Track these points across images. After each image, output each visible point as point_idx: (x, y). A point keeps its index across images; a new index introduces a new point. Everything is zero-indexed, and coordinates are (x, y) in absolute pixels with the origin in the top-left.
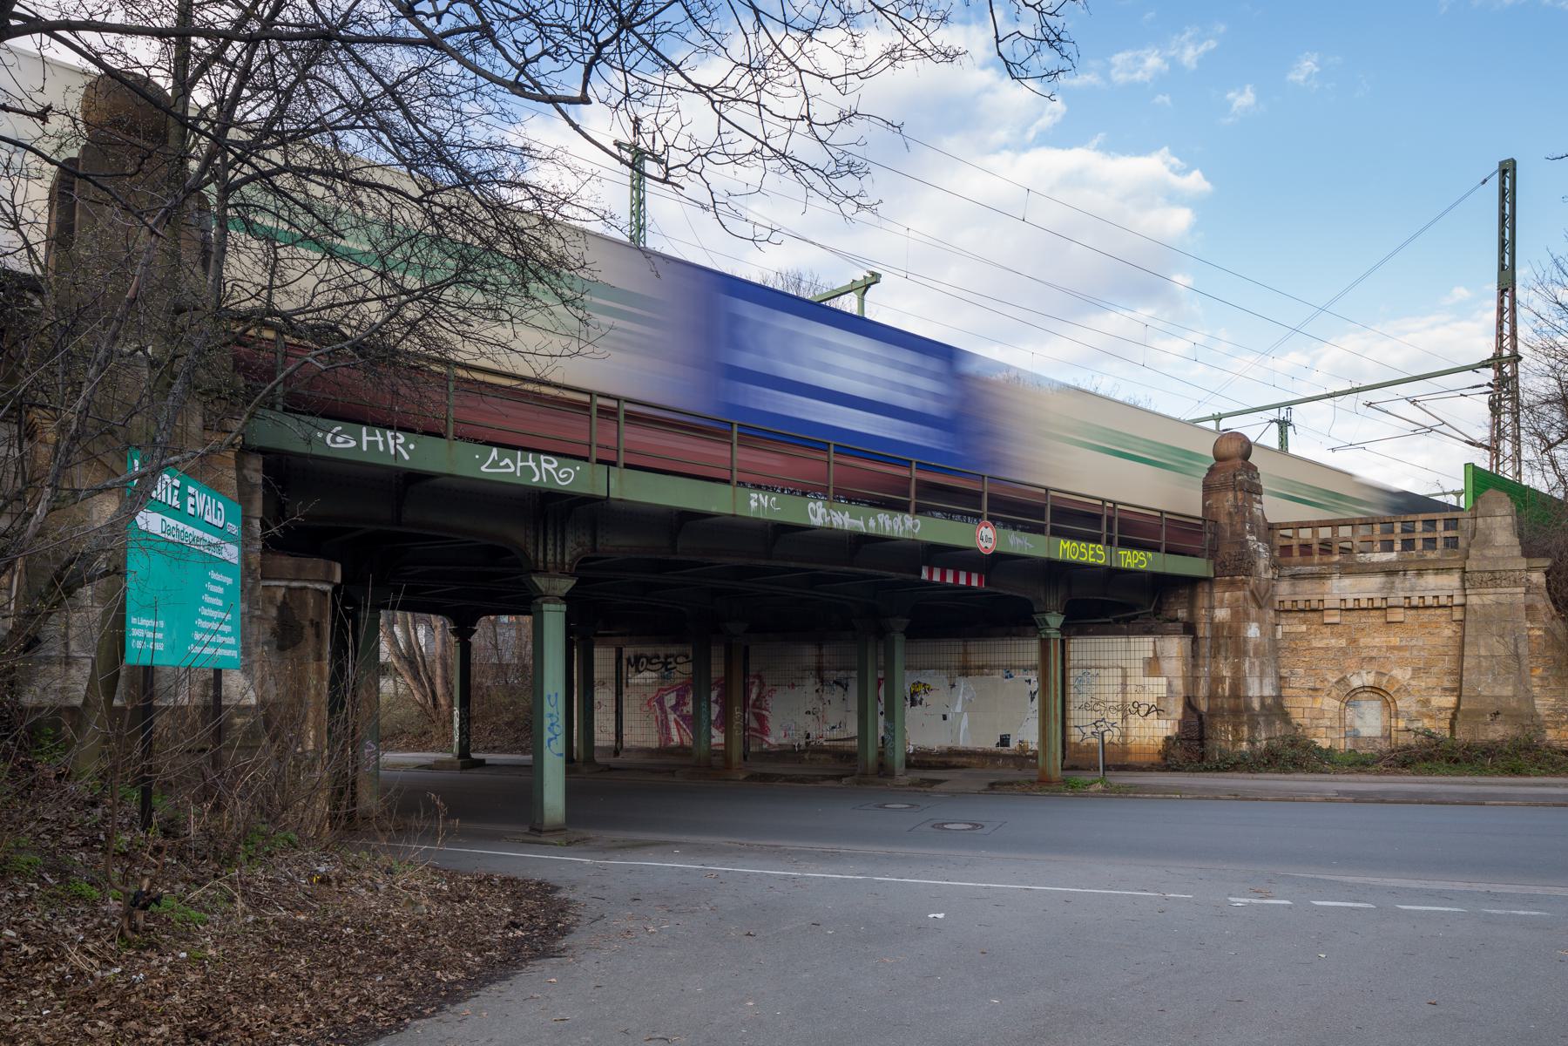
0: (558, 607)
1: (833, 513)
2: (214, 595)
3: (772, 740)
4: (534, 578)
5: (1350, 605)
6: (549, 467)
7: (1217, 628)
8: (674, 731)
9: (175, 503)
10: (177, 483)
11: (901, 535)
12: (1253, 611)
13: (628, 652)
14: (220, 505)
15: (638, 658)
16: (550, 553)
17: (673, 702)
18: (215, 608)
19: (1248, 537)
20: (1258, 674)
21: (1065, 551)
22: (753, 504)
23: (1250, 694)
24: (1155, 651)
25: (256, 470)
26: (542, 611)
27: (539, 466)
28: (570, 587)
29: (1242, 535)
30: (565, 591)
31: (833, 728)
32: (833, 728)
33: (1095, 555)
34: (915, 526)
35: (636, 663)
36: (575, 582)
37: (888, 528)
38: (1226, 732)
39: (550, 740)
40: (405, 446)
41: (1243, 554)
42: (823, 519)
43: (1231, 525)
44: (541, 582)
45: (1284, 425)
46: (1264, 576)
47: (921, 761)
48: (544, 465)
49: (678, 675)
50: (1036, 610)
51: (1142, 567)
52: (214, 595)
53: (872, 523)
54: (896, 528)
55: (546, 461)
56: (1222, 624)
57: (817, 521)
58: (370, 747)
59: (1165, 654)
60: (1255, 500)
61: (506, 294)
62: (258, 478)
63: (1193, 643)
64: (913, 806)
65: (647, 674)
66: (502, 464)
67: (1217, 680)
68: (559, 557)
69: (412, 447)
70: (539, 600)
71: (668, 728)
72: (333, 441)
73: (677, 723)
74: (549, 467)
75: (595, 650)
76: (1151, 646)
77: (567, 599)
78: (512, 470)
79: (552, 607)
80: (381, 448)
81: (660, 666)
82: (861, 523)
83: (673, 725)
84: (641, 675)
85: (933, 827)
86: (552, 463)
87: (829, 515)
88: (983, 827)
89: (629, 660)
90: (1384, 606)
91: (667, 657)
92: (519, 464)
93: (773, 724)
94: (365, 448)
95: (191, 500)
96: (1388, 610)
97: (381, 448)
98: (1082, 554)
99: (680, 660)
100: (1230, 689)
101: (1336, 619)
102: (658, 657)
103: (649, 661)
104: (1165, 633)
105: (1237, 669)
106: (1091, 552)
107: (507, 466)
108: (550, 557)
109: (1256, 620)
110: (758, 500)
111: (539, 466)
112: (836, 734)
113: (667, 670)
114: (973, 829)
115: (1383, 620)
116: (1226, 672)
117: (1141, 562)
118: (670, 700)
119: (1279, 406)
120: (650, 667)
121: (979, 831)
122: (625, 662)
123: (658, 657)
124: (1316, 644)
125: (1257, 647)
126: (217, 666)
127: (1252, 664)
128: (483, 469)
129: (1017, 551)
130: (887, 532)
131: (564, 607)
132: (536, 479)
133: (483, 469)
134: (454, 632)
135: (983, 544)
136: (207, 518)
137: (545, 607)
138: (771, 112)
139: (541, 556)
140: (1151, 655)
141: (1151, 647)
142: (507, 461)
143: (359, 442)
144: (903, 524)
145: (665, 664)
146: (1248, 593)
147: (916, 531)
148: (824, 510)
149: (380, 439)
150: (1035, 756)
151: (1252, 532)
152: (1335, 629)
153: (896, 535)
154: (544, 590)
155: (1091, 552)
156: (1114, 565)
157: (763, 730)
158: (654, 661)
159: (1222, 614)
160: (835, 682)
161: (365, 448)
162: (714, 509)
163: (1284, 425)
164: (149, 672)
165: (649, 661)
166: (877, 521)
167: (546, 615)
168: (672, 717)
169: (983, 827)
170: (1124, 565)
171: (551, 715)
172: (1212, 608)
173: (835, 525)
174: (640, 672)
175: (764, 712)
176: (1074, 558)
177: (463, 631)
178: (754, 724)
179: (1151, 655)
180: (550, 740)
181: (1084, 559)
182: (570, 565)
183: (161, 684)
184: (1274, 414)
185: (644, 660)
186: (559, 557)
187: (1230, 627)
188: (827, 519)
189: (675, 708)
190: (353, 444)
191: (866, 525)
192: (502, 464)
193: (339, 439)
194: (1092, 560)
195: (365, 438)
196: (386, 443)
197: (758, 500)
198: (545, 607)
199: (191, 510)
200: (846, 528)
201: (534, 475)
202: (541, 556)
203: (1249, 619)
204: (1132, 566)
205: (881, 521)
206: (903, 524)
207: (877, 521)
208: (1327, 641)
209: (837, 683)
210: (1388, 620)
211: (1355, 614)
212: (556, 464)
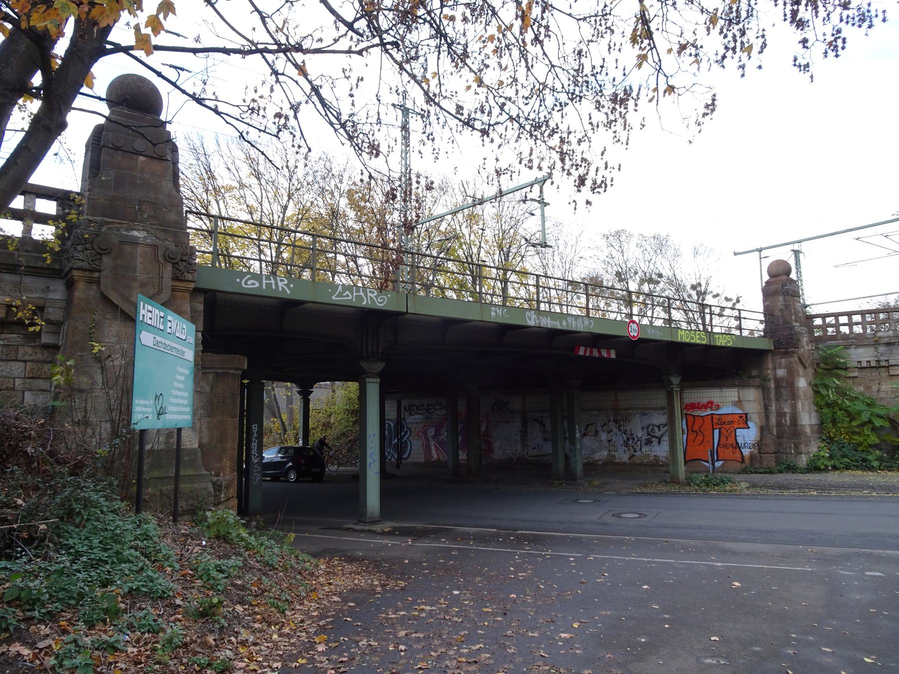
0: (375, 380)
1: (541, 318)
2: (179, 381)
3: (496, 457)
4: (361, 363)
5: (864, 365)
6: (372, 295)
7: (778, 381)
8: (434, 452)
9: (162, 327)
10: (162, 314)
11: (582, 330)
12: (801, 371)
13: (404, 403)
14: (184, 326)
15: (410, 406)
16: (370, 347)
17: (433, 433)
18: (179, 389)
19: (794, 324)
20: (807, 410)
21: (681, 337)
22: (493, 314)
23: (804, 423)
24: (739, 397)
25: (200, 303)
26: (365, 383)
27: (366, 295)
28: (142, 296)
29: (790, 323)
30: (379, 370)
31: (534, 448)
32: (534, 448)
33: (700, 339)
34: (590, 324)
35: (410, 409)
37: (574, 326)
38: (790, 448)
39: (371, 464)
40: (287, 285)
41: (792, 334)
43: (783, 317)
44: (365, 365)
45: (797, 253)
46: (806, 348)
47: (591, 467)
48: (369, 294)
49: (435, 416)
51: (729, 345)
52: (179, 381)
53: (564, 323)
54: (579, 325)
55: (370, 292)
56: (782, 379)
57: (531, 323)
58: (257, 469)
59: (746, 399)
60: (796, 300)
62: (201, 307)
63: (763, 392)
64: (595, 501)
65: (416, 416)
66: (344, 294)
67: (780, 415)
68: (375, 349)
70: (364, 376)
71: (430, 450)
72: (246, 283)
73: (436, 447)
74: (372, 295)
75: (386, 402)
76: (736, 394)
77: (380, 375)
78: (350, 298)
79: (372, 380)
80: (274, 287)
81: (424, 411)
82: (558, 324)
83: (433, 448)
84: (413, 417)
85: (613, 515)
87: (538, 319)
88: (646, 516)
89: (405, 408)
90: (887, 365)
91: (428, 405)
92: (355, 294)
93: (496, 445)
94: (264, 288)
95: (169, 324)
96: (890, 368)
97: (274, 287)
98: (692, 338)
99: (437, 407)
100: (791, 420)
101: (856, 374)
102: (423, 406)
103: (418, 408)
104: (748, 386)
105: (794, 407)
106: (698, 337)
107: (348, 296)
108: (370, 349)
109: (803, 376)
110: (496, 312)
111: (366, 295)
112: (535, 452)
113: (429, 413)
114: (640, 517)
115: (887, 374)
116: (787, 410)
117: (729, 342)
118: (431, 432)
119: (793, 243)
120: (418, 412)
121: (644, 519)
122: (402, 409)
123: (423, 406)
125: (805, 393)
126: (179, 427)
127: (803, 404)
128: (333, 298)
129: (652, 337)
130: (574, 328)
131: (378, 380)
132: (364, 303)
133: (333, 298)
134: (300, 393)
135: (632, 334)
136: (178, 335)
137: (367, 380)
138: (226, 51)
139: (364, 349)
140: (737, 399)
141: (737, 395)
142: (347, 292)
143: (261, 284)
144: (583, 323)
145: (428, 410)
146: (797, 359)
147: (591, 327)
148: (535, 316)
149: (273, 281)
150: (665, 465)
151: (796, 321)
152: (856, 381)
153: (579, 330)
154: (366, 369)
155: (698, 337)
156: (712, 344)
157: (490, 450)
158: (421, 408)
159: (781, 373)
160: (534, 419)
161: (264, 288)
162: (470, 318)
163: (797, 253)
164: (143, 432)
165: (418, 408)
166: (567, 322)
167: (368, 385)
168: (432, 443)
169: (646, 516)
170: (718, 344)
171: (372, 448)
172: (775, 369)
174: (412, 415)
175: (492, 440)
176: (688, 340)
177: (305, 395)
178: (484, 447)
179: (737, 399)
180: (371, 464)
181: (693, 341)
183: (147, 437)
184: (791, 247)
185: (415, 408)
186: (375, 349)
187: (787, 381)
188: (537, 322)
189: (434, 437)
190: (257, 285)
191: (561, 323)
192: (344, 294)
193: (250, 282)
194: (698, 342)
196: (276, 284)
197: (496, 312)
198: (367, 380)
199: (169, 330)
200: (549, 326)
202: (364, 349)
203: (799, 375)
204: (723, 344)
205: (570, 321)
206: (583, 323)
207: (567, 322)
209: (536, 420)
210: (891, 374)
211: (868, 370)
212: (376, 294)
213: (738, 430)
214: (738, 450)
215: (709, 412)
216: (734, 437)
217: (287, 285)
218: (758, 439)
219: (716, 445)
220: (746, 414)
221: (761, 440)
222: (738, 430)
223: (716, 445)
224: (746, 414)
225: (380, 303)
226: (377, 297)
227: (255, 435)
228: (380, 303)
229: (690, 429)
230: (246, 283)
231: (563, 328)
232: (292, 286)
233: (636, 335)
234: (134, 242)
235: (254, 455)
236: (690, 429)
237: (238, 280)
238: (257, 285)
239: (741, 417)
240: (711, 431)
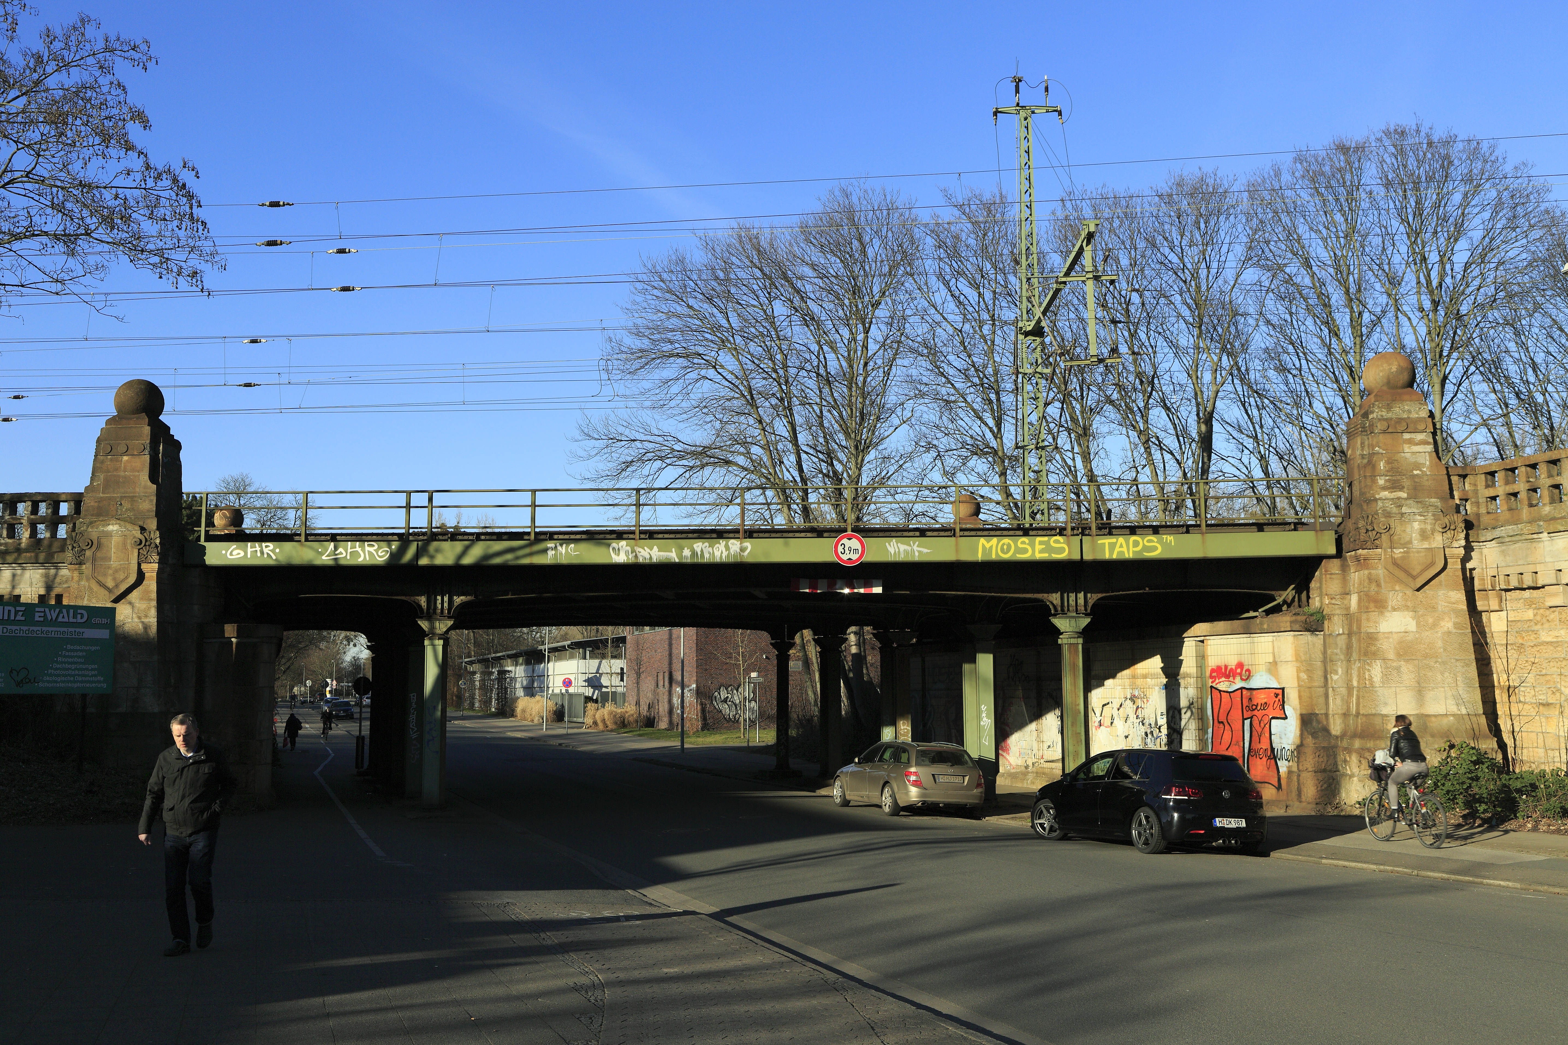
4: (419, 622)
6: (372, 549)
36: (452, 622)
37: (707, 555)
40: (273, 551)
42: (627, 556)
50: (1462, 549)
61: (912, 275)
69: (277, 550)
86: (373, 546)
92: (349, 550)
124: (1545, 637)
132: (360, 560)
143: (246, 553)
156: (1088, 557)
173: (641, 560)
182: (1089, 492)
191: (680, 555)
195: (249, 550)
200: (654, 560)
201: (360, 556)
208: (1556, 633)
212: (376, 547)
213: (1273, 721)
214: (1273, 761)
215: (1239, 684)
216: (1267, 735)
217: (273, 551)
218: (1298, 742)
219: (1246, 755)
220: (1283, 689)
221: (1302, 742)
222: (1273, 721)
223: (1246, 755)
224: (1283, 689)
225: (380, 557)
226: (377, 551)
227: (415, 706)
228: (380, 557)
229: (1216, 718)
230: (231, 554)
231: (684, 561)
232: (277, 550)
233: (854, 557)
234: (109, 535)
235: (413, 729)
236: (1216, 718)
237: (224, 552)
238: (242, 554)
239: (1277, 695)
240: (1241, 721)
